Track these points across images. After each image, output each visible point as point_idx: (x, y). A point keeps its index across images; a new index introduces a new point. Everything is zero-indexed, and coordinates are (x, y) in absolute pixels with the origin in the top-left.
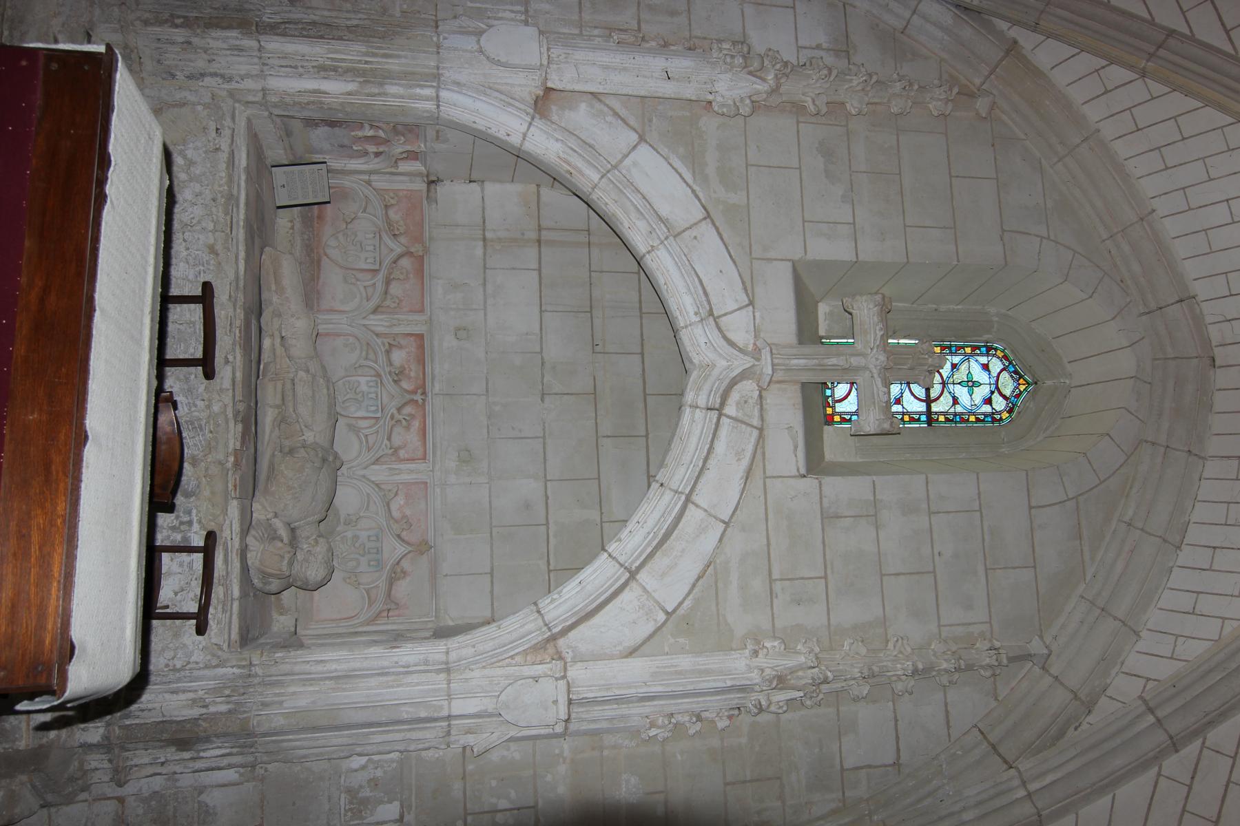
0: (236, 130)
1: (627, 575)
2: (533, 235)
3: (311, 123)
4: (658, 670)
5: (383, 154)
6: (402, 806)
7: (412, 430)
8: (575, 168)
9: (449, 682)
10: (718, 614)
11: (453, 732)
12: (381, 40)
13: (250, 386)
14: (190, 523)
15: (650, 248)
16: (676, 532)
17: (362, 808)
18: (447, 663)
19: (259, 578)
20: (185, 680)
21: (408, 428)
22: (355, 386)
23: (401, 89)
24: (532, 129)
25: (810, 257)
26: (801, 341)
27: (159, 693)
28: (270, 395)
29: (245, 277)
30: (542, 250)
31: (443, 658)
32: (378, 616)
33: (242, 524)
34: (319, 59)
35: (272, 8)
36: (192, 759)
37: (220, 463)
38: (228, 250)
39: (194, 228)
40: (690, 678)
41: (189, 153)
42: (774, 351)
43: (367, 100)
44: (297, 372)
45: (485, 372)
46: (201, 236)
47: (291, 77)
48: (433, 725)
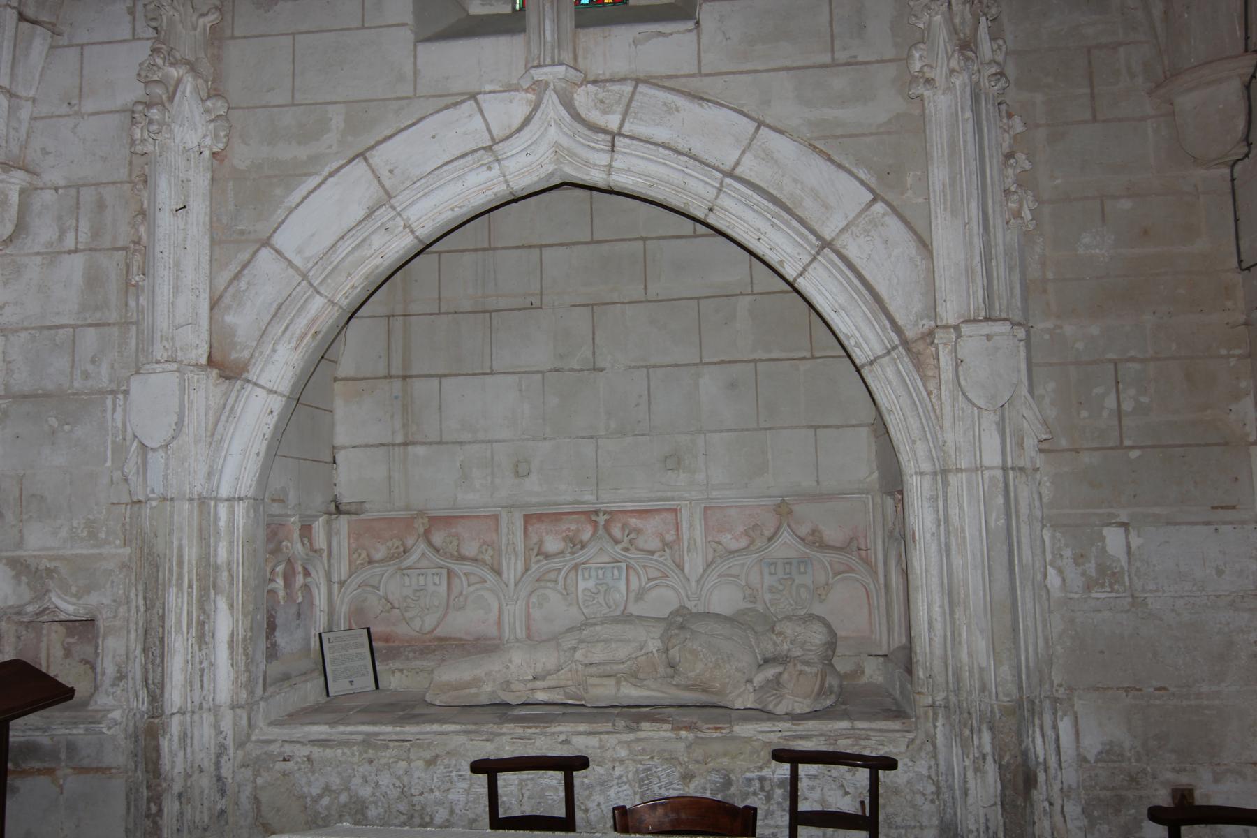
0: (284, 739)
1: (827, 250)
2: (398, 384)
3: (272, 652)
4: (949, 210)
5: (307, 567)
6: (1109, 525)
7: (642, 526)
8: (309, 327)
9: (960, 470)
10: (877, 134)
11: (1021, 464)
12: (161, 569)
13: (594, 715)
14: (762, 779)
15: (407, 230)
16: (771, 190)
17: (1109, 572)
18: (935, 474)
19: (825, 699)
20: (950, 780)
21: (638, 531)
22: (590, 594)
23: (221, 544)
24: (261, 382)
25: (409, 18)
26: (523, 30)
27: (967, 809)
28: (604, 691)
29: (463, 724)
30: (414, 373)
31: (928, 480)
32: (866, 562)
33: (762, 720)
34: (190, 642)
35: (132, 700)
36: (1046, 771)
37: (689, 747)
38: (431, 743)
39: (406, 783)
40: (960, 167)
41: (315, 791)
42: (536, 63)
43: (238, 584)
44: (576, 661)
45: (568, 440)
46: (415, 776)
47: (215, 675)
48: (1012, 489)
